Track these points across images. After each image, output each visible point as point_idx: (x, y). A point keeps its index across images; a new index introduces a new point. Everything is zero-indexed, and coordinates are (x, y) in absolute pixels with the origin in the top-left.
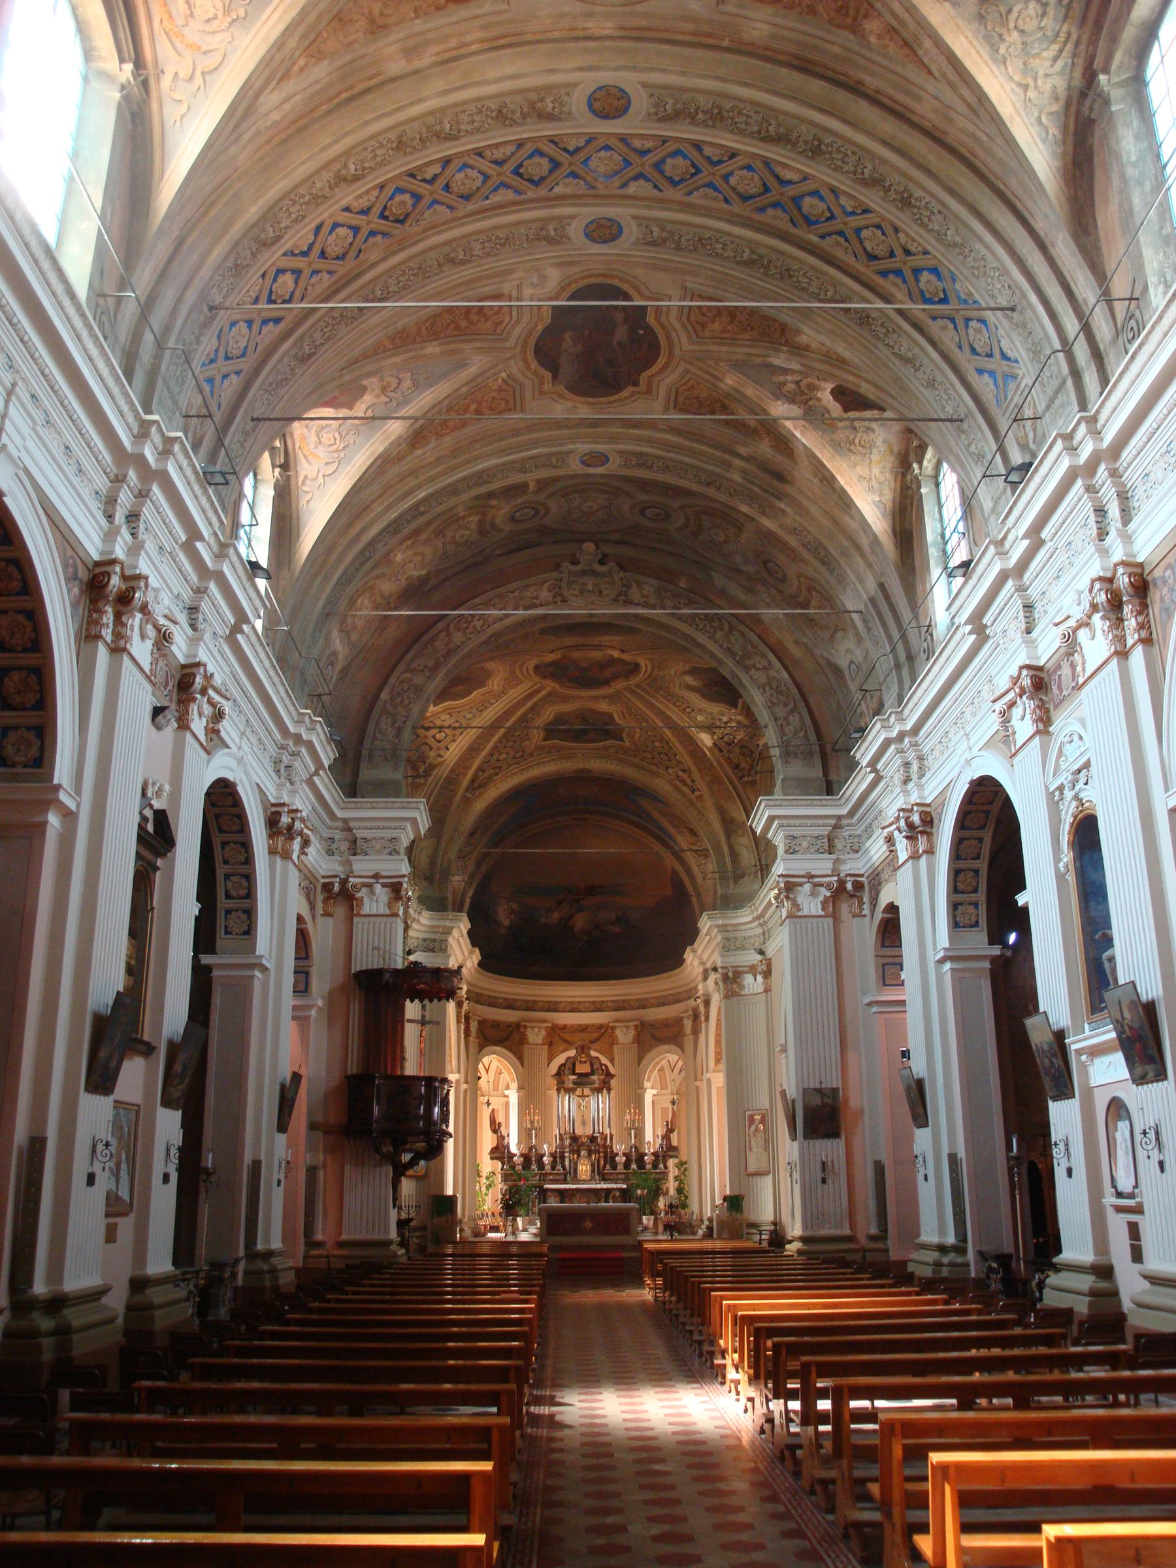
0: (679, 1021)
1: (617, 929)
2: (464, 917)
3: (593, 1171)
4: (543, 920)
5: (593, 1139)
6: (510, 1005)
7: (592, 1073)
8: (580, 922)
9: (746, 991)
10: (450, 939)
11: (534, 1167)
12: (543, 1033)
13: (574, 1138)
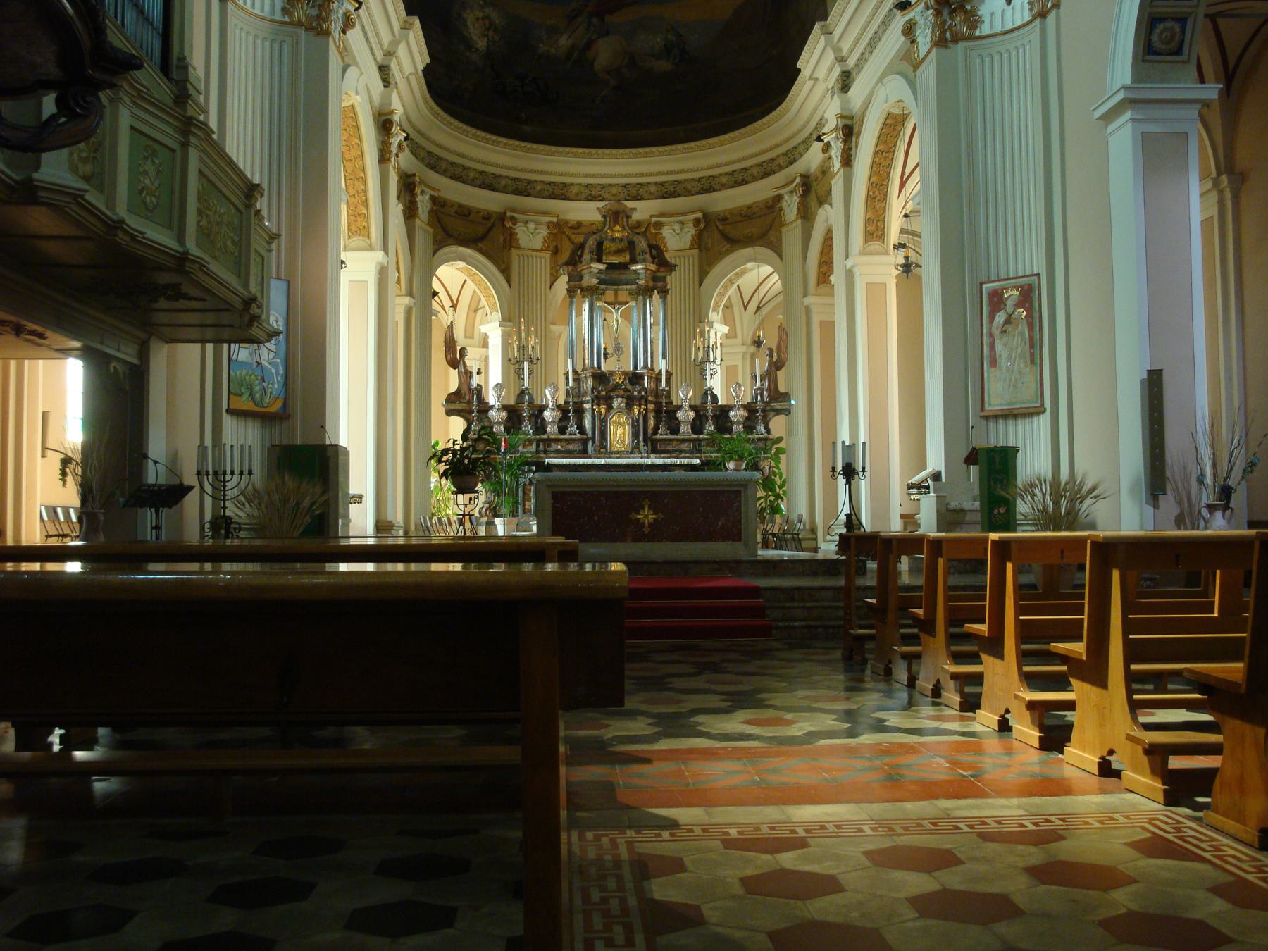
0: (773, 206)
1: (663, 65)
3: (635, 435)
4: (542, 48)
5: (635, 378)
6: (489, 183)
7: (634, 261)
8: (605, 54)
9: (985, 29)
11: (527, 428)
12: (544, 232)
13: (600, 378)
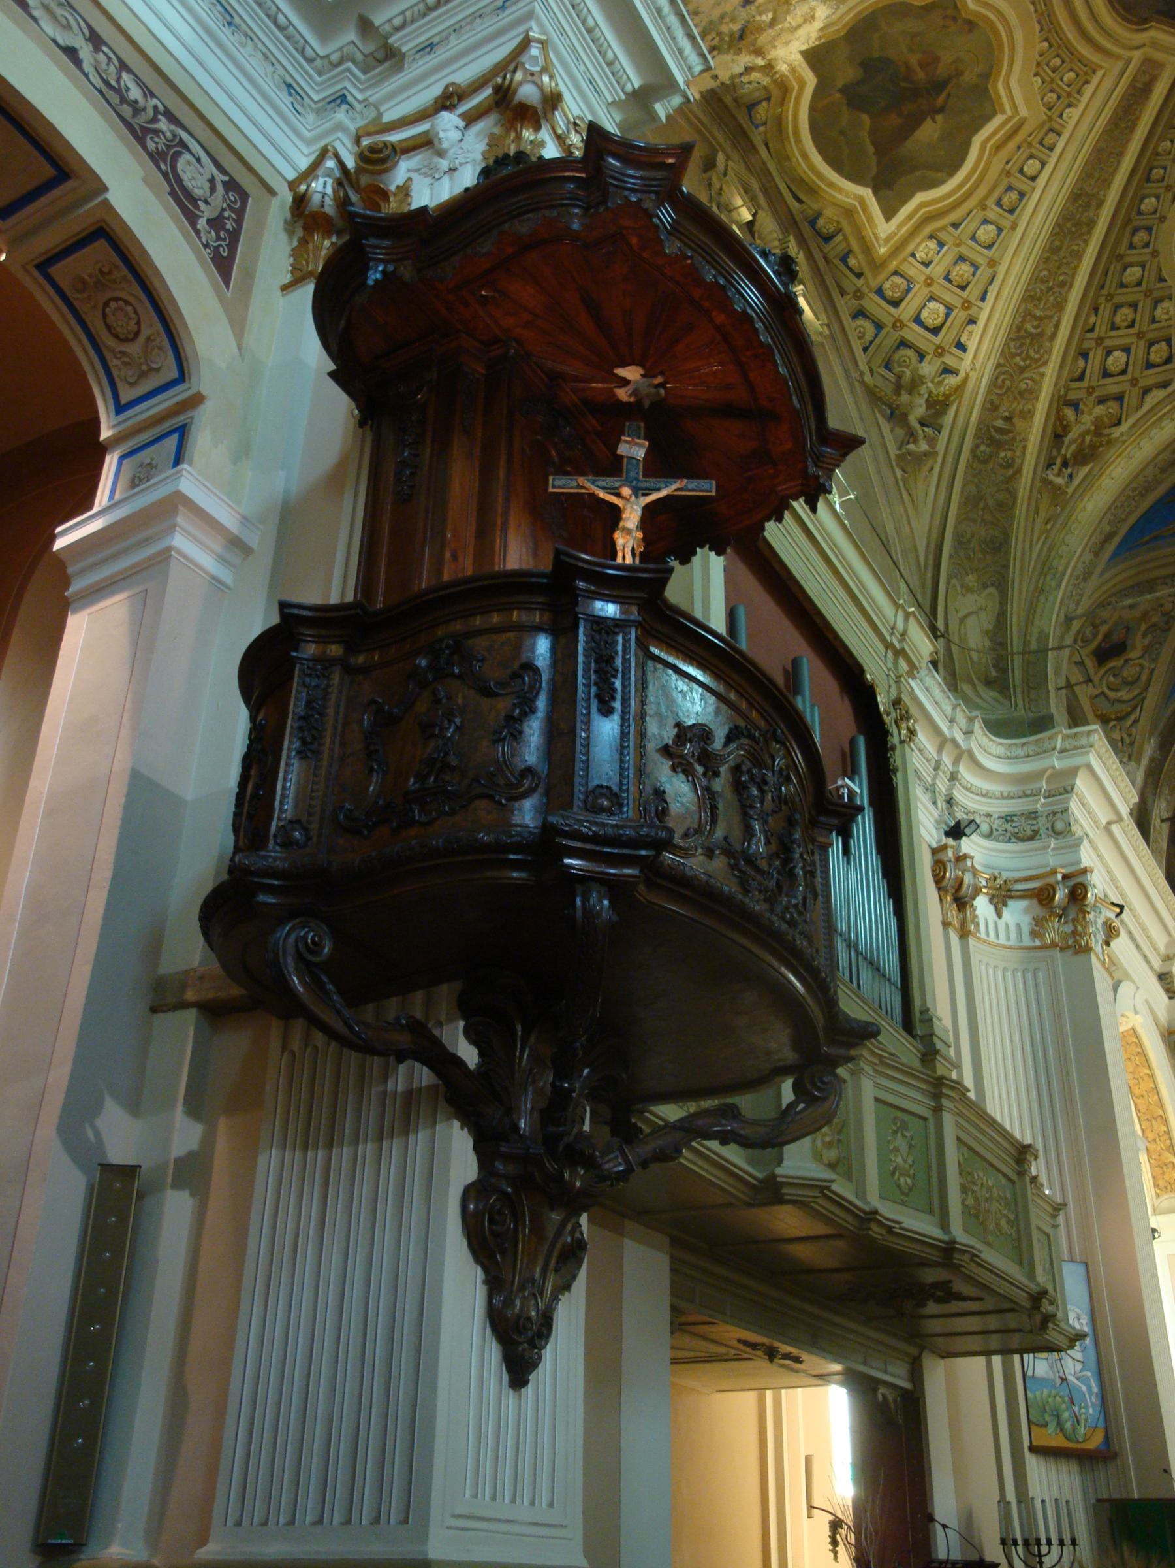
2: (1096, 734)
10: (1074, 806)
